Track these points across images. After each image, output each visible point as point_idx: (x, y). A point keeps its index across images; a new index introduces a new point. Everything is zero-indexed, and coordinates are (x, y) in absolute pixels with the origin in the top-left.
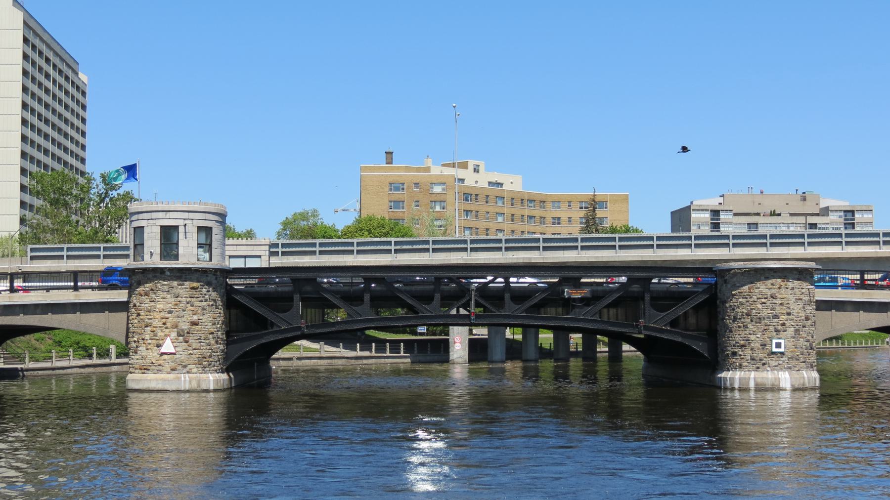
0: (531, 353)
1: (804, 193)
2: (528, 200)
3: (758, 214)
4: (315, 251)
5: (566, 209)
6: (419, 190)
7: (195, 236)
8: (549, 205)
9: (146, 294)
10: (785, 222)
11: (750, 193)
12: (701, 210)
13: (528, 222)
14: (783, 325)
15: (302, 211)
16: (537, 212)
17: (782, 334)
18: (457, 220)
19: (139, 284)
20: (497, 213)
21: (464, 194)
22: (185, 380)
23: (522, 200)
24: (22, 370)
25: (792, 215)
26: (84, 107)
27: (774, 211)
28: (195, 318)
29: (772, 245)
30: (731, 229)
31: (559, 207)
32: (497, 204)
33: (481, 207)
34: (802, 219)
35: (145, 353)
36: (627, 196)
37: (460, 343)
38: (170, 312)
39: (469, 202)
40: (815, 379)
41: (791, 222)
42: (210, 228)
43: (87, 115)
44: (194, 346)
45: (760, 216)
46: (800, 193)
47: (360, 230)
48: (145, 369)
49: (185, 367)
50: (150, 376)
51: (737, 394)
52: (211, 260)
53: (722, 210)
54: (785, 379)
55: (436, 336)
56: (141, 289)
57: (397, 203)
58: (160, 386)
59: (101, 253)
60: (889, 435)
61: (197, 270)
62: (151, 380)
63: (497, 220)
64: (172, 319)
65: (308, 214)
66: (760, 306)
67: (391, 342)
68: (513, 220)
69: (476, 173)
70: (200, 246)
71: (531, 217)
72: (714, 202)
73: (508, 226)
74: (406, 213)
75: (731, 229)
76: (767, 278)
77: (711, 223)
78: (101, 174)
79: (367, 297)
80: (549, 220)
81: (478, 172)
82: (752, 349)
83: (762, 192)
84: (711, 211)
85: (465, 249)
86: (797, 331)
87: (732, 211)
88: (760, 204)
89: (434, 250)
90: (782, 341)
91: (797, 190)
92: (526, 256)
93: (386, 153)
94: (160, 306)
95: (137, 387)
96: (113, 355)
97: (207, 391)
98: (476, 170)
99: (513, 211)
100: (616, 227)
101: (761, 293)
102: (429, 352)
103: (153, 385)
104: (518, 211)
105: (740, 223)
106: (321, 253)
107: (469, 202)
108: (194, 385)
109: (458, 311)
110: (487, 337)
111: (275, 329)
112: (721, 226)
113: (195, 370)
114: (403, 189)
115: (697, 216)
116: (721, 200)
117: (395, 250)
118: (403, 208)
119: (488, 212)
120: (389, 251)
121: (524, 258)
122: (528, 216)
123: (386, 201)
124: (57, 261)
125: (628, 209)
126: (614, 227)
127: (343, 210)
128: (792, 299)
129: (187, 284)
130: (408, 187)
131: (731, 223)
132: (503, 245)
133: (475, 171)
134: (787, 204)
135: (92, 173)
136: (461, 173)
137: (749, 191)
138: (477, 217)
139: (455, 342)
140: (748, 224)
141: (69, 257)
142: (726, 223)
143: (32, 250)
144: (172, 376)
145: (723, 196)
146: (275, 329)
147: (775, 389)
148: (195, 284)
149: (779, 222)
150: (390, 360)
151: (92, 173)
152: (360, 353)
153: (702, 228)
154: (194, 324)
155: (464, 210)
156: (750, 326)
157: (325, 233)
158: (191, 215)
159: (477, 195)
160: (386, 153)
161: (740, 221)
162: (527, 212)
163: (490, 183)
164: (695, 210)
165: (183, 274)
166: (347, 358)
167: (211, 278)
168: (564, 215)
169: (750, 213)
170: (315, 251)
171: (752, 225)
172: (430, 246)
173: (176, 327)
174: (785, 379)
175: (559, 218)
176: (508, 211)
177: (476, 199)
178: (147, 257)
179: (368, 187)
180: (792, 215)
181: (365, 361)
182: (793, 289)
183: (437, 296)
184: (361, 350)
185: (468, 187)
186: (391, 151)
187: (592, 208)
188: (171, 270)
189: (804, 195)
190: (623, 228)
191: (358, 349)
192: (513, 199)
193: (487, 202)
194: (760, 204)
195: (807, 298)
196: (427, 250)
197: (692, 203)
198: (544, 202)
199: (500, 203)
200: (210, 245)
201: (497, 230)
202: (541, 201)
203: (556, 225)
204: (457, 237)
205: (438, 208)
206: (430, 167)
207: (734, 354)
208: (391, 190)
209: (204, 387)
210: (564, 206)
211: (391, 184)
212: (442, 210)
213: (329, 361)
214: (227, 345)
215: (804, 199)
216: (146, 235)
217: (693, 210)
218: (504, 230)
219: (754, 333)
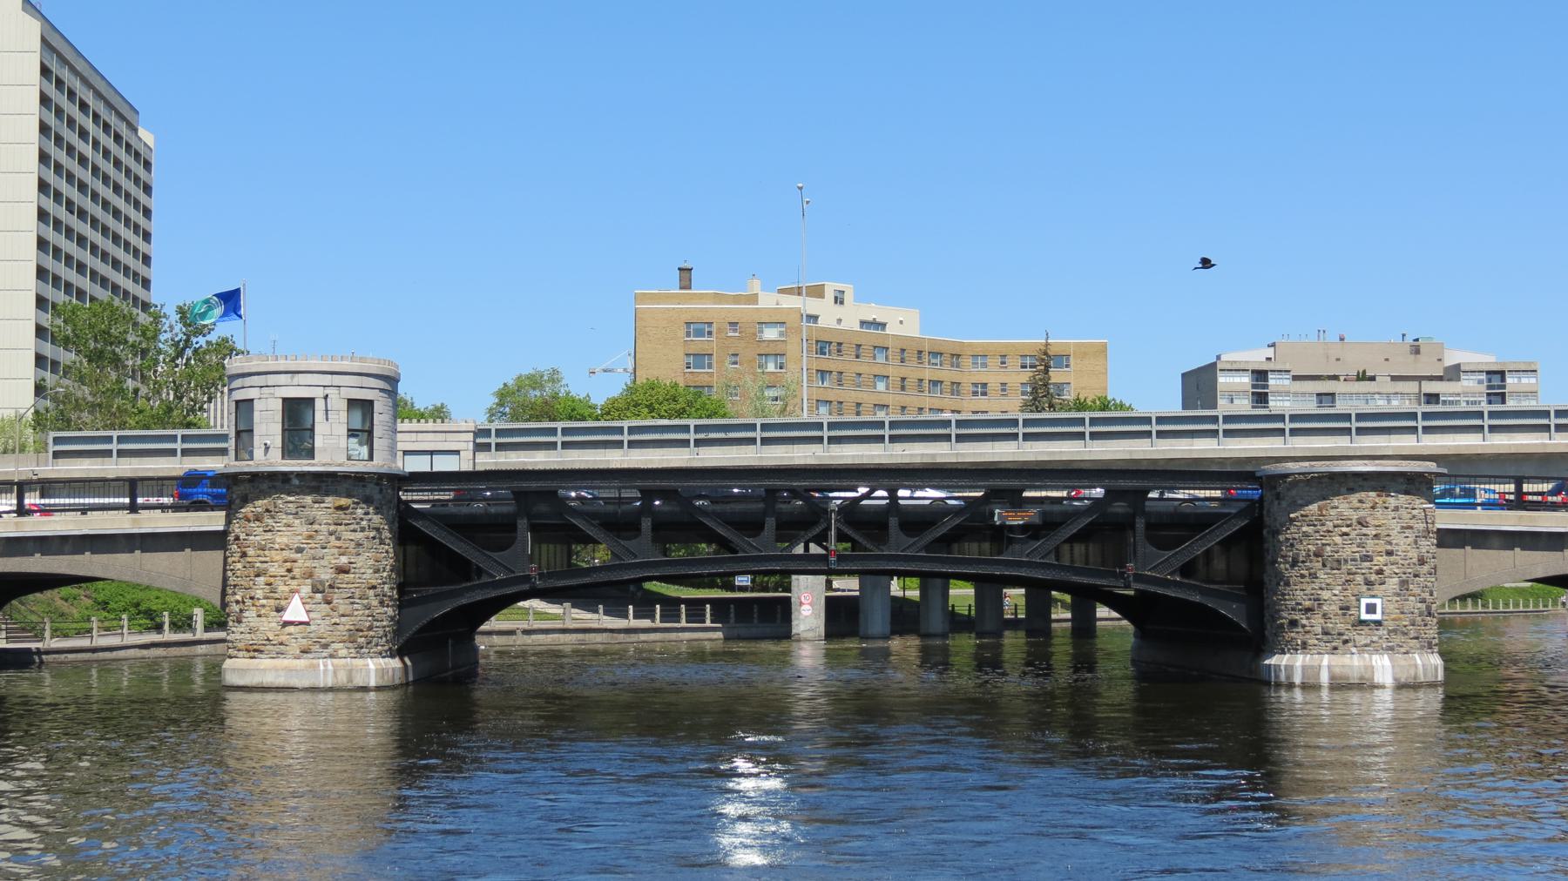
0: (936, 622)
1: (1417, 340)
3: (1335, 378)
5: (997, 369)
7: (344, 415)
8: (967, 362)
9: (258, 518)
14: (1380, 572)
15: (532, 372)
16: (947, 374)
17: (1378, 589)
19: (245, 500)
20: (875, 376)
21: (817, 342)
22: (326, 671)
23: (920, 352)
24: (39, 652)
25: (1394, 378)
26: (147, 189)
27: (1364, 372)
28: (344, 560)
29: (1360, 431)
30: (1287, 404)
31: (984, 365)
32: (875, 359)
34: (1412, 387)
35: (255, 623)
37: (810, 604)
38: (299, 550)
41: (1394, 391)
42: (371, 402)
43: (154, 203)
44: (342, 609)
45: (1339, 380)
46: (1409, 340)
47: (635, 406)
48: (254, 651)
50: (264, 662)
51: (1298, 695)
52: (371, 458)
54: (1383, 668)
56: (247, 510)
58: (281, 681)
59: (178, 446)
62: (266, 670)
64: (302, 563)
66: (1338, 539)
67: (688, 602)
68: (903, 388)
70: (352, 433)
71: (935, 383)
72: (1257, 357)
74: (715, 376)
75: (1287, 404)
76: (1351, 491)
77: (1253, 393)
78: (178, 307)
79: (646, 524)
81: (842, 303)
82: (1324, 615)
83: (1342, 339)
84: (1253, 372)
85: (820, 440)
86: (1404, 584)
88: (1338, 360)
89: (765, 441)
90: (1378, 601)
91: (1404, 335)
93: (679, 269)
94: (281, 540)
96: (199, 626)
97: (365, 689)
98: (839, 300)
99: (904, 372)
101: (1340, 516)
102: (756, 621)
103: (269, 679)
104: (912, 372)
105: (1304, 394)
106: (565, 445)
108: (342, 679)
109: (807, 548)
110: (857, 593)
111: (485, 579)
112: (1270, 398)
113: (343, 652)
114: (710, 333)
116: (1270, 352)
118: (710, 366)
120: (685, 443)
122: (930, 381)
123: (681, 355)
124: (100, 460)
127: (605, 371)
128: (1395, 527)
129: (330, 501)
130: (719, 331)
131: (1287, 393)
132: (887, 432)
133: (836, 302)
134: (1387, 360)
135: (162, 306)
136: (812, 305)
140: (1318, 395)
142: (1279, 393)
143: (57, 441)
145: (1273, 345)
146: (485, 579)
147: (1366, 685)
148: (344, 501)
149: (1372, 390)
150: (687, 635)
151: (162, 306)
152: (634, 623)
153: (1236, 402)
154: (342, 570)
155: (818, 371)
156: (1321, 574)
157: (573, 410)
158: (337, 380)
159: (840, 344)
160: (679, 269)
161: (1303, 390)
162: (928, 374)
163: (863, 323)
165: (323, 483)
166: (612, 631)
167: (372, 490)
168: (993, 378)
172: (758, 434)
173: (311, 576)
174: (1383, 668)
175: (985, 385)
176: (895, 371)
177: (839, 351)
178: (258, 453)
180: (1394, 378)
181: (643, 637)
182: (1396, 509)
183: (770, 523)
187: (1043, 367)
188: (301, 475)
189: (1416, 343)
190: (1098, 402)
191: (631, 616)
192: (903, 350)
193: (857, 357)
194: (1338, 360)
195: (1422, 526)
196: (752, 441)
199: (881, 359)
200: (370, 432)
202: (953, 355)
204: (805, 417)
205: (771, 367)
208: (688, 334)
210: (994, 363)
212: (779, 370)
213: (580, 636)
215: (1416, 351)
216: (256, 415)
218: (888, 406)
219: (1328, 587)
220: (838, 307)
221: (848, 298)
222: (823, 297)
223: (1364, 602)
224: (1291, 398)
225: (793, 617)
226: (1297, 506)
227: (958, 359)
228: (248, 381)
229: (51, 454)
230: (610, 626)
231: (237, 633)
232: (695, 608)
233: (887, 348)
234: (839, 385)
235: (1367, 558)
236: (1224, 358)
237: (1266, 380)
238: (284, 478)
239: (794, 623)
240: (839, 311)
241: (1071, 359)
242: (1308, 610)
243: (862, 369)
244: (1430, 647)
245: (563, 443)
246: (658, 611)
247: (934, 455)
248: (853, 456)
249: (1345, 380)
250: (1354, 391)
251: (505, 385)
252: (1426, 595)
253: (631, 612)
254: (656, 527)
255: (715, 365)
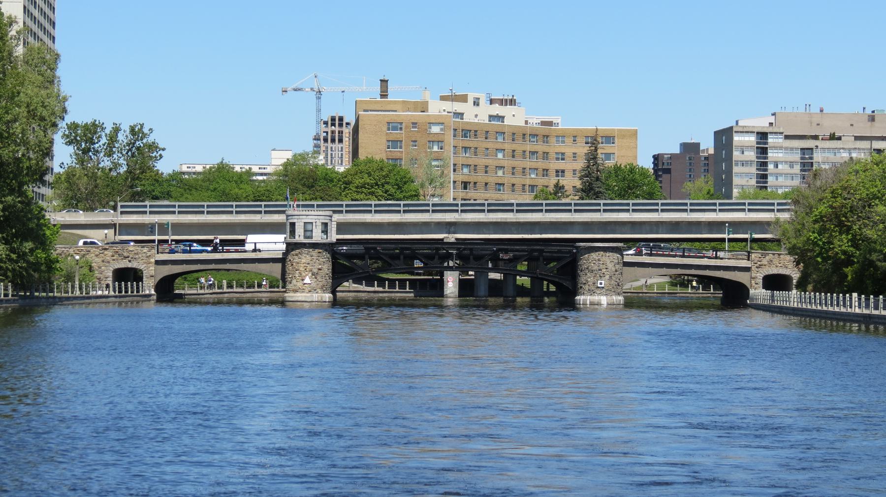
0: (510, 291)
1: (873, 112)
2: (530, 135)
3: (815, 137)
4: (343, 211)
5: (571, 144)
6: (416, 129)
7: (320, 227)
8: (553, 140)
9: (297, 255)
10: (845, 147)
11: (808, 111)
12: (746, 132)
14: (604, 274)
16: (540, 148)
17: (603, 278)
19: (293, 250)
20: (497, 149)
21: (462, 130)
22: (315, 297)
23: (524, 135)
24: (185, 295)
25: (857, 138)
26: (53, 24)
27: (834, 133)
28: (320, 266)
30: (781, 155)
31: (563, 142)
32: (497, 139)
33: (480, 143)
34: (865, 144)
35: (295, 283)
36: (636, 131)
37: (452, 282)
38: (308, 264)
39: (468, 139)
41: (853, 147)
44: (320, 280)
46: (868, 112)
47: (360, 173)
48: (296, 291)
49: (315, 290)
50: (298, 294)
51: (582, 306)
52: (327, 238)
53: (770, 133)
54: (604, 300)
56: (293, 252)
58: (303, 299)
59: (177, 210)
60: (885, 385)
62: (299, 296)
64: (309, 267)
65: (308, 155)
66: (592, 265)
67: (399, 280)
68: (513, 156)
69: (476, 107)
70: (323, 232)
71: (533, 153)
72: (762, 123)
73: (508, 163)
74: (403, 153)
75: (781, 155)
76: (596, 251)
77: (757, 148)
78: (130, 126)
79: (402, 257)
80: (552, 155)
81: (478, 105)
83: (822, 111)
84: (758, 133)
85: (457, 211)
86: (611, 277)
87: (782, 133)
89: (434, 211)
90: (603, 282)
91: (864, 108)
94: (303, 261)
95: (292, 300)
96: (225, 287)
97: (325, 302)
98: (476, 103)
102: (428, 289)
103: (300, 299)
104: (519, 147)
105: (792, 149)
106: (347, 212)
107: (468, 139)
108: (320, 299)
109: (448, 264)
110: (473, 277)
112: (769, 151)
113: (320, 292)
114: (401, 129)
116: (772, 119)
117: (403, 210)
118: (401, 148)
119: (488, 149)
120: (399, 212)
121: (501, 218)
122: (530, 152)
123: (384, 141)
124: (141, 215)
126: (619, 166)
127: (295, 90)
128: (608, 261)
129: (317, 250)
130: (406, 127)
131: (781, 148)
132: (486, 208)
133: (474, 104)
134: (852, 125)
135: (120, 124)
136: (458, 107)
137: (806, 108)
138: (476, 154)
139: (448, 282)
141: (151, 213)
142: (775, 148)
143: (122, 207)
144: (309, 295)
145: (774, 114)
147: (599, 304)
148: (320, 251)
150: (399, 295)
151: (120, 124)
152: (376, 289)
154: (320, 269)
155: (462, 147)
156: (588, 274)
157: (326, 175)
158: (319, 217)
159: (476, 131)
160: (381, 80)
161: (791, 146)
162: (529, 147)
163: (490, 116)
164: (738, 132)
165: (315, 246)
166: (368, 292)
167: (327, 247)
168: (569, 150)
170: (343, 211)
171: (806, 151)
172: (431, 208)
173: (311, 271)
174: (604, 300)
175: (563, 154)
176: (508, 147)
177: (475, 135)
178: (297, 237)
179: (365, 126)
180: (857, 138)
181: (381, 295)
183: (437, 257)
184: (378, 286)
185: (467, 123)
186: (386, 79)
187: (594, 148)
190: (628, 167)
191: (376, 286)
192: (514, 134)
193: (486, 138)
195: (617, 261)
196: (428, 211)
197: (737, 122)
198: (547, 136)
199: (500, 139)
200: (327, 231)
201: (497, 167)
202: (544, 136)
203: (560, 161)
204: (452, 201)
205: (436, 148)
206: (428, 101)
207: (581, 287)
208: (389, 129)
210: (569, 140)
211: (388, 123)
212: (440, 150)
213: (356, 294)
214: (332, 280)
215: (872, 118)
217: (735, 132)
218: (504, 167)
219: (590, 278)
222: (467, 102)
223: (599, 282)
225: (445, 287)
228: (294, 217)
229: (119, 213)
230: (368, 290)
232: (402, 283)
233: (504, 133)
235: (600, 270)
236: (740, 124)
237: (767, 139)
239: (445, 290)
240: (476, 110)
241: (616, 139)
242: (585, 284)
243: (489, 145)
244: (619, 294)
247: (506, 218)
248: (472, 218)
249: (822, 139)
250: (827, 147)
252: (618, 280)
253: (376, 284)
254: (405, 258)
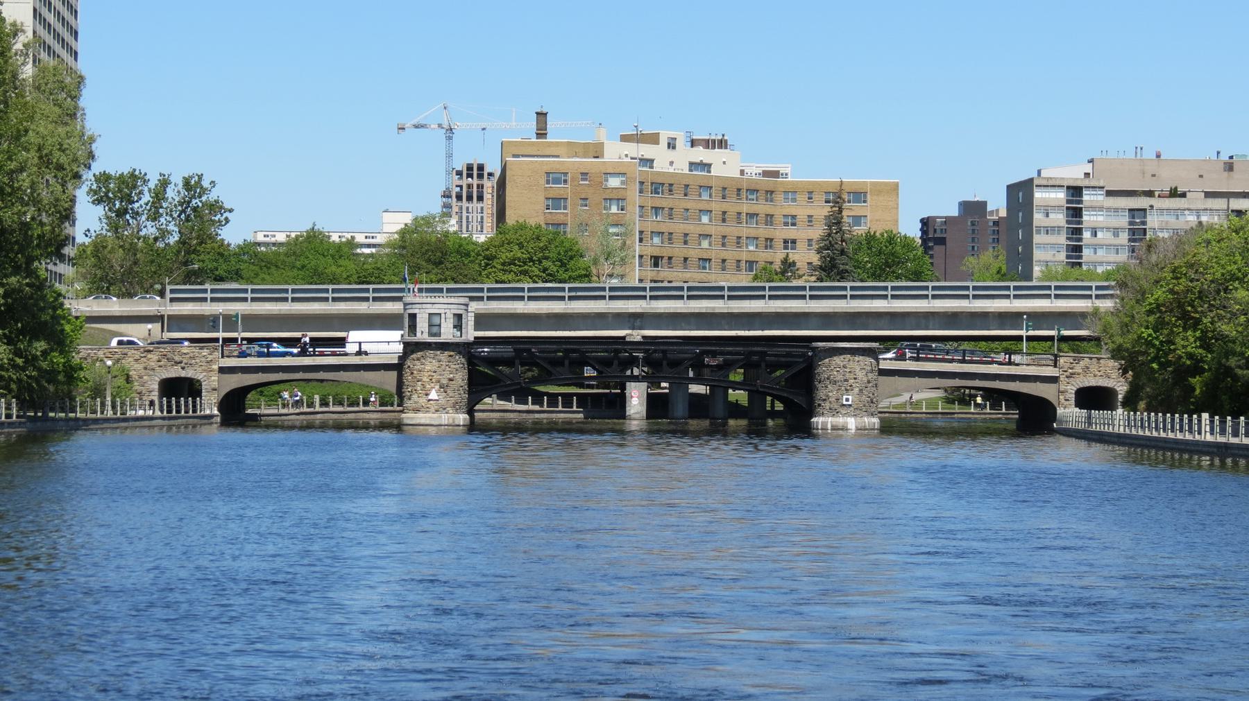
0: (720, 410)
1: (1231, 157)
2: (747, 190)
3: (1150, 194)
4: (483, 297)
7: (452, 320)
8: (779, 197)
9: (418, 359)
13: (747, 223)
15: (426, 214)
16: (762, 208)
17: (851, 392)
18: (637, 271)
20: (700, 211)
21: (652, 183)
22: (445, 418)
23: (739, 190)
24: (261, 415)
25: (1208, 195)
26: (75, 34)
27: (1176, 188)
28: (451, 376)
29: (975, 297)
30: (1101, 218)
31: (794, 200)
32: (700, 196)
33: (677, 201)
34: (1220, 204)
35: (416, 400)
38: (435, 372)
39: (660, 195)
40: (874, 423)
41: (1203, 207)
42: (461, 315)
43: (80, 46)
44: (451, 395)
45: (1154, 196)
46: (1224, 157)
47: (508, 244)
48: (417, 410)
49: (445, 409)
50: (420, 415)
51: (820, 431)
52: (461, 336)
53: (1086, 187)
54: (851, 423)
55: (387, 406)
56: (414, 356)
57: (557, 202)
58: (428, 422)
61: (452, 344)
62: (422, 418)
63: (700, 221)
65: (434, 219)
66: (835, 373)
67: (562, 395)
68: (724, 220)
70: (455, 327)
71: (751, 216)
72: (1074, 173)
74: (566, 215)
75: (1101, 218)
76: (841, 354)
77: (1068, 208)
78: (184, 178)
80: (779, 219)
81: (674, 148)
82: (830, 402)
83: (1158, 156)
84: (1068, 188)
85: (644, 297)
86: (861, 390)
87: (1103, 187)
88: (1154, 175)
89: (611, 298)
90: (850, 397)
91: (1218, 153)
92: (709, 306)
93: (537, 113)
94: (428, 368)
95: (411, 423)
97: (459, 425)
98: (671, 145)
99: (725, 207)
100: (875, 233)
101: (836, 364)
103: (423, 421)
104: (732, 207)
105: (1116, 210)
106: (489, 298)
108: (451, 421)
110: (667, 391)
111: (502, 384)
112: (1084, 213)
113: (451, 411)
114: (565, 181)
115: (1044, 196)
116: (1088, 168)
119: (688, 210)
120: (562, 298)
121: (707, 307)
122: (747, 214)
123: (542, 198)
125: (898, 204)
127: (416, 127)
128: (858, 369)
131: (1101, 208)
133: (669, 147)
134: (1201, 176)
135: (169, 175)
136: (646, 151)
137: (1136, 153)
138: (671, 216)
140: (1131, 210)
141: (213, 300)
142: (1093, 208)
143: (172, 291)
145: (1091, 161)
146: (502, 384)
147: (844, 429)
148: (452, 353)
149: (1182, 206)
150: (562, 415)
151: (169, 175)
152: (531, 407)
153: (1051, 216)
154: (451, 380)
155: (652, 208)
157: (460, 246)
158: (450, 306)
159: (671, 185)
160: (537, 113)
161: (1116, 206)
162: (745, 208)
163: (691, 164)
164: (1040, 186)
165: (444, 346)
166: (519, 411)
168: (802, 212)
169: (1137, 191)
170: (483, 297)
173: (439, 382)
174: (851, 423)
175: (794, 217)
176: (717, 207)
177: (670, 191)
178: (419, 334)
179: (515, 178)
180: (1208, 195)
181: (537, 416)
182: (858, 361)
183: (616, 362)
184: (533, 404)
186: (544, 111)
188: (436, 343)
189: (1231, 161)
190: (885, 235)
191: (530, 403)
192: (724, 189)
194: (1154, 175)
195: (869, 368)
196: (603, 297)
198: (772, 192)
199: (705, 196)
200: (461, 326)
201: (700, 235)
202: (767, 192)
203: (790, 227)
204: (637, 284)
205: (614, 209)
207: (819, 405)
208: (548, 182)
209: (457, 423)
210: (802, 198)
211: (548, 174)
212: (620, 212)
213: (502, 414)
216: (418, 319)
217: (1037, 186)
220: (671, 152)
221: (679, 144)
224: (1105, 213)
226: (821, 360)
227: (771, 194)
228: (414, 306)
230: (518, 409)
231: (408, 404)
232: (567, 399)
233: (711, 187)
234: (670, 219)
235: (846, 380)
236: (1044, 174)
237: (1081, 195)
238: (430, 344)
239: (627, 409)
240: (671, 155)
241: (868, 196)
242: (825, 400)
244: (872, 415)
245: (487, 297)
246: (545, 400)
248: (665, 308)
251: (406, 225)
252: (871, 395)
255: (569, 207)
